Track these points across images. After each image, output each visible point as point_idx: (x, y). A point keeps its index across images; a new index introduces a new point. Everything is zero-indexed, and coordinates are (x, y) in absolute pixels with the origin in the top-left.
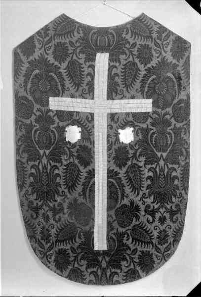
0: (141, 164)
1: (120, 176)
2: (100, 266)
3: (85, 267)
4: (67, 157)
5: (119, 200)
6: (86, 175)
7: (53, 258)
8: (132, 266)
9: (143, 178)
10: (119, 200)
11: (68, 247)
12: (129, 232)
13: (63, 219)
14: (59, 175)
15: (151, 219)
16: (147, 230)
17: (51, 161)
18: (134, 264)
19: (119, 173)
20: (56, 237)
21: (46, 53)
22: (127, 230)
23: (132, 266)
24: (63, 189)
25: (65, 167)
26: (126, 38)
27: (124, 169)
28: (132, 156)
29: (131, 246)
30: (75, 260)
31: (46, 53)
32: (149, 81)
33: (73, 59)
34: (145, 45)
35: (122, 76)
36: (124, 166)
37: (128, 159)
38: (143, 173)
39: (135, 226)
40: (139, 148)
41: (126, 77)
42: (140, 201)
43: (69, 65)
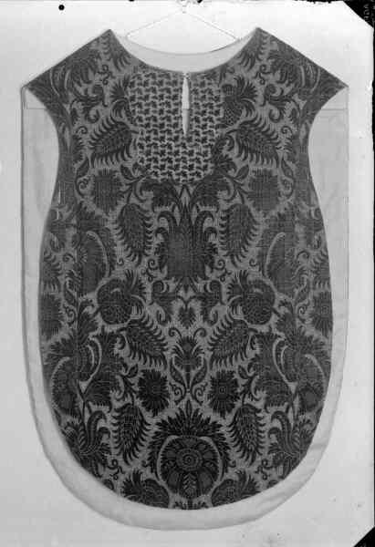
0: (259, 405)
1: (222, 430)
2: (178, 203)
3: (149, 202)
4: (119, 394)
5: (220, 474)
6: (156, 429)
7: (89, 187)
8: (238, 200)
9: (263, 432)
10: (220, 474)
11: (117, 167)
12: (234, 135)
13: (102, 117)
14: (107, 429)
15: (276, 112)
16: (270, 132)
17: (90, 403)
18: (241, 196)
19: (220, 426)
20: (91, 149)
21: (80, 193)
22: (229, 133)
23: (238, 200)
24: (104, 61)
25: (117, 414)
26: (230, 156)
27: (230, 417)
28: (244, 391)
29: (236, 161)
30: (130, 191)
31: (80, 193)
32: (274, 242)
33: (131, 202)
34: (265, 171)
35: (222, 233)
36: (230, 411)
37: (236, 397)
38: (262, 422)
39: (246, 123)
40: (255, 375)
41: (229, 235)
42: (255, 77)
43: (124, 212)
